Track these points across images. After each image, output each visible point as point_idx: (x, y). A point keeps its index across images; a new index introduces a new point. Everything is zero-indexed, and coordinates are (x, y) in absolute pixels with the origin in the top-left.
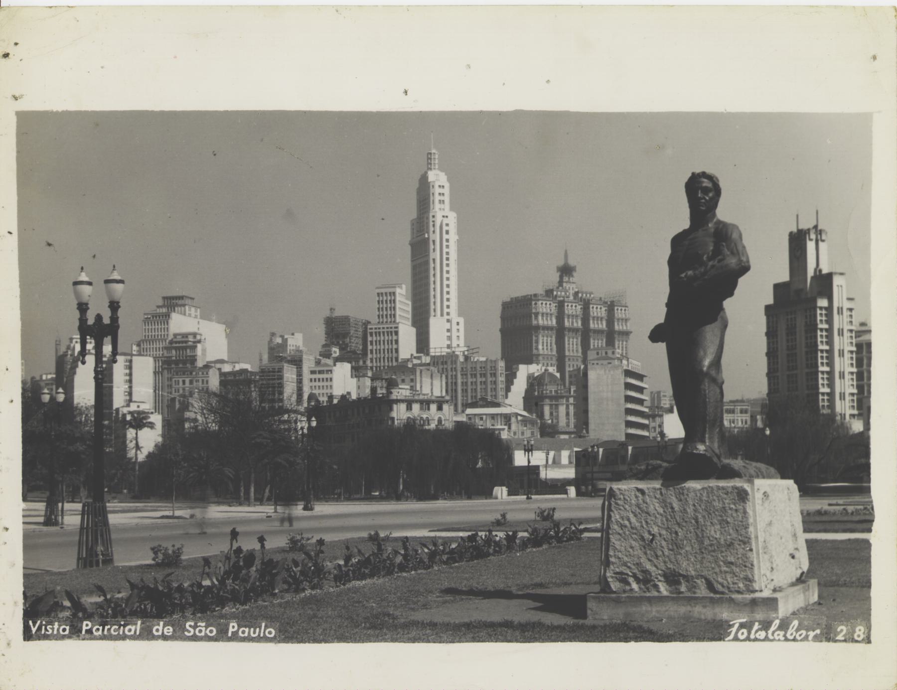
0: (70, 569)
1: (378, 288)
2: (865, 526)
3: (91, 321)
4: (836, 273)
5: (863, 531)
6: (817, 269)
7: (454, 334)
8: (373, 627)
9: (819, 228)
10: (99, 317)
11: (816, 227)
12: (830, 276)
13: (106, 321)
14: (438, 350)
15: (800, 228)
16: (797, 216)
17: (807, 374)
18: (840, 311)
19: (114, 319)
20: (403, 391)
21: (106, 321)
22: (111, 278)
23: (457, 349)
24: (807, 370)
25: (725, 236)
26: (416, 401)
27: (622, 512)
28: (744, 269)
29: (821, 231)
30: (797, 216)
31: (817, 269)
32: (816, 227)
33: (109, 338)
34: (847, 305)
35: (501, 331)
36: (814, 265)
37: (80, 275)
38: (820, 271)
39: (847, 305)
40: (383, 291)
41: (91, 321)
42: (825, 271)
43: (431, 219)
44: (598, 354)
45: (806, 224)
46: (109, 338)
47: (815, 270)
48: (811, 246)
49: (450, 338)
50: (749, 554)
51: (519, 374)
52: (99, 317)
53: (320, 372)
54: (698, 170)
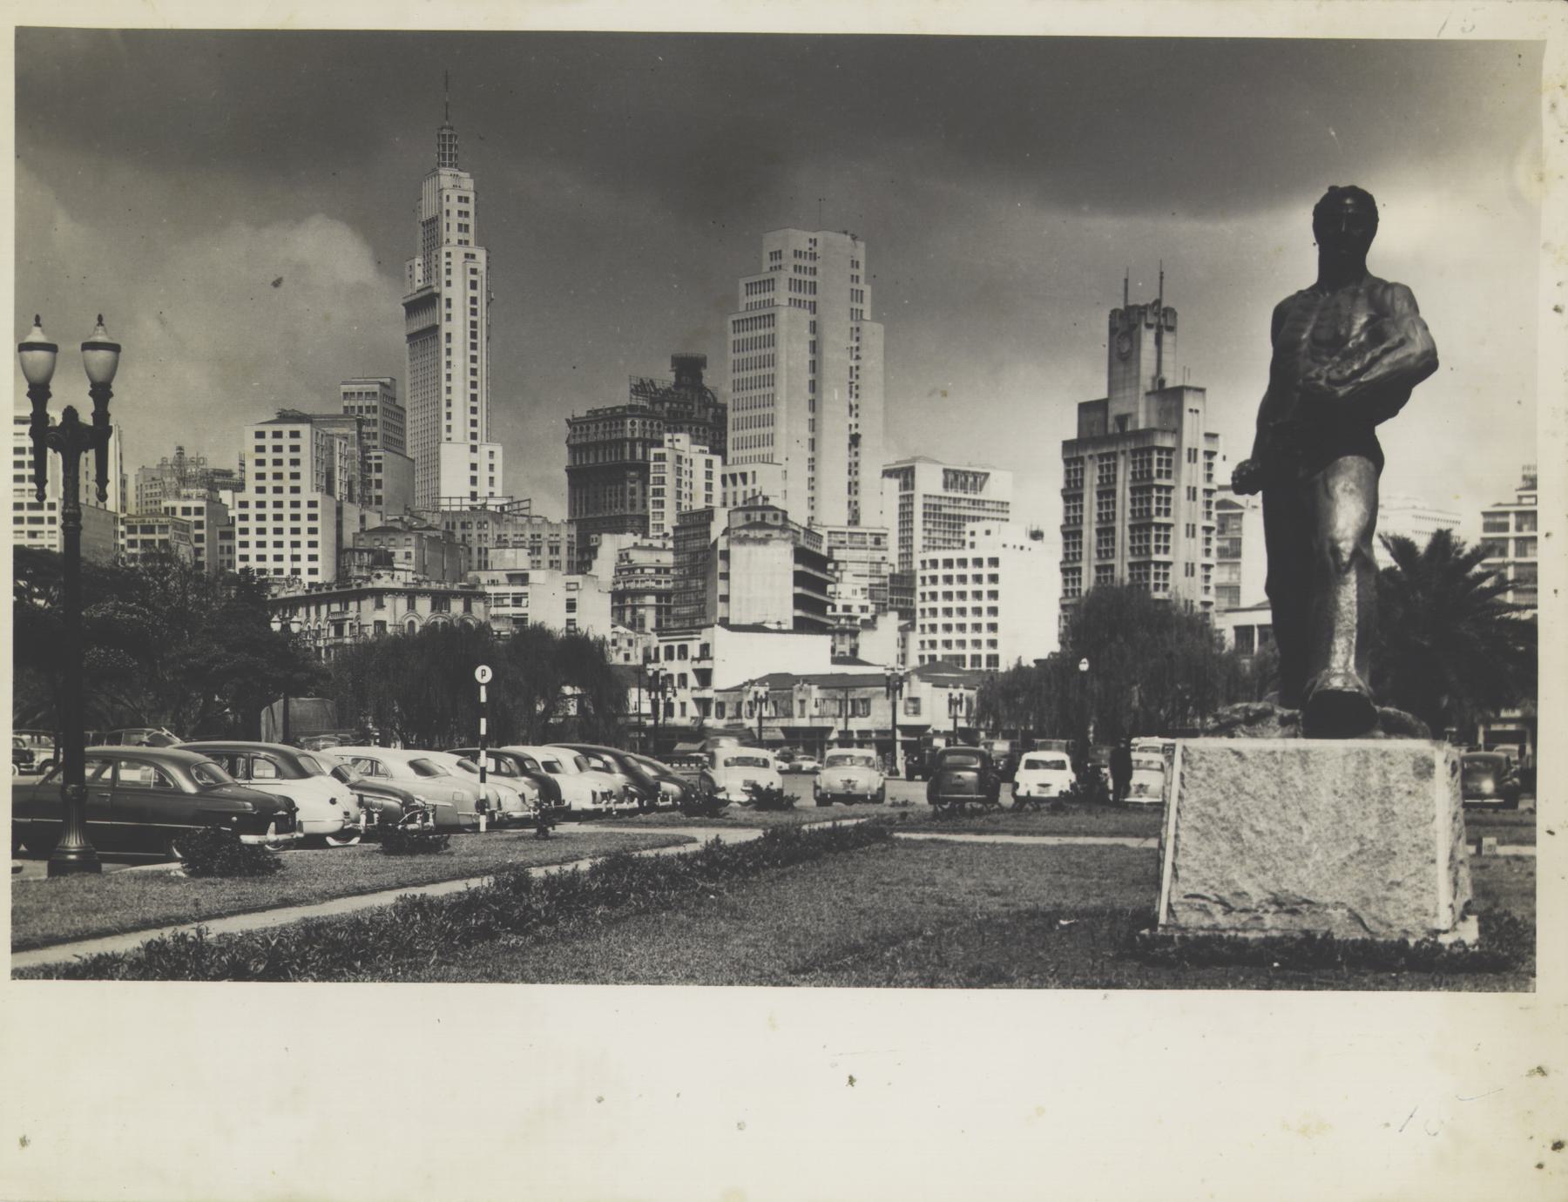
0: (1442, 794)
1: (344, 383)
2: (1524, 832)
3: (56, 415)
4: (1189, 388)
5: (1521, 842)
7: (483, 474)
8: (833, 969)
9: (1164, 304)
10: (70, 413)
11: (1158, 302)
13: (86, 417)
16: (1126, 281)
17: (1131, 565)
19: (101, 415)
20: (402, 574)
21: (86, 417)
22: (92, 339)
23: (490, 502)
24: (1131, 560)
25: (1391, 307)
26: (424, 593)
28: (1428, 364)
29: (1166, 310)
30: (1126, 281)
32: (1158, 302)
33: (91, 454)
34: (1203, 446)
36: (1153, 371)
39: (1203, 446)
41: (56, 415)
43: (444, 260)
44: (748, 517)
45: (1143, 295)
46: (91, 454)
48: (1148, 338)
49: (474, 480)
50: (1430, 869)
52: (70, 413)
53: (954, 517)
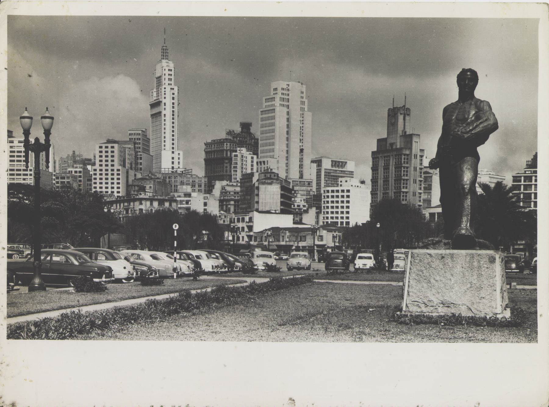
3: (32, 140)
4: (414, 134)
6: (404, 132)
7: (176, 161)
10: (37, 140)
11: (404, 106)
12: (411, 136)
13: (42, 141)
14: (167, 170)
15: (395, 106)
18: (416, 156)
19: (47, 140)
21: (42, 141)
22: (45, 115)
24: (394, 191)
26: (156, 200)
27: (417, 267)
31: (404, 132)
33: (44, 153)
35: (205, 160)
37: (23, 113)
38: (405, 132)
40: (133, 132)
41: (32, 140)
42: (408, 133)
45: (399, 104)
46: (44, 153)
47: (403, 131)
48: (401, 118)
49: (173, 163)
51: (216, 187)
52: (37, 140)
53: (335, 176)
54: (467, 68)
